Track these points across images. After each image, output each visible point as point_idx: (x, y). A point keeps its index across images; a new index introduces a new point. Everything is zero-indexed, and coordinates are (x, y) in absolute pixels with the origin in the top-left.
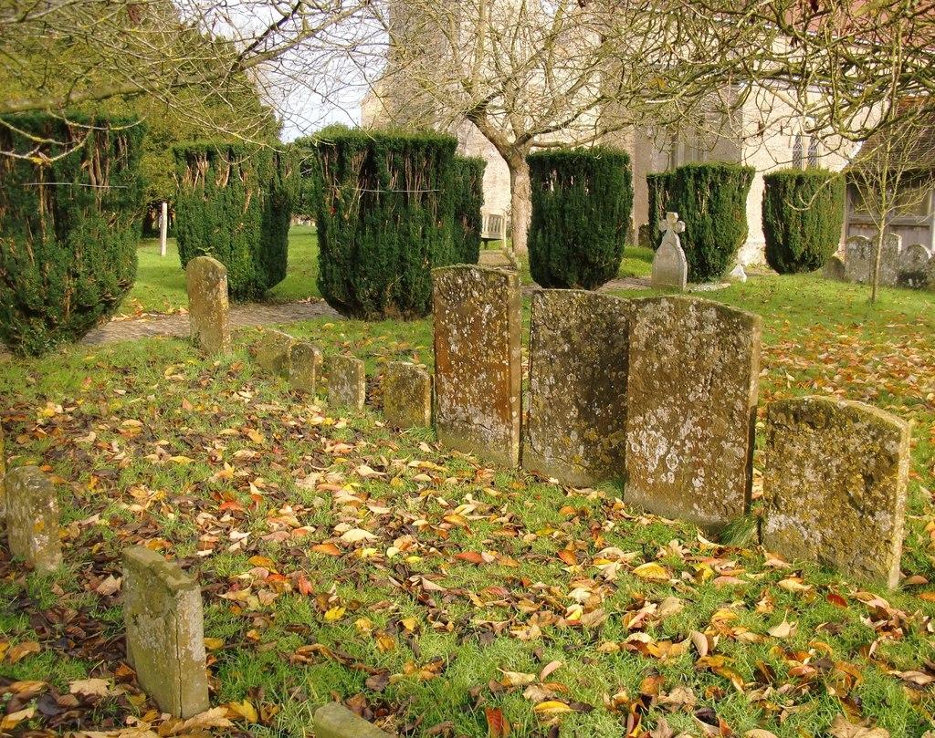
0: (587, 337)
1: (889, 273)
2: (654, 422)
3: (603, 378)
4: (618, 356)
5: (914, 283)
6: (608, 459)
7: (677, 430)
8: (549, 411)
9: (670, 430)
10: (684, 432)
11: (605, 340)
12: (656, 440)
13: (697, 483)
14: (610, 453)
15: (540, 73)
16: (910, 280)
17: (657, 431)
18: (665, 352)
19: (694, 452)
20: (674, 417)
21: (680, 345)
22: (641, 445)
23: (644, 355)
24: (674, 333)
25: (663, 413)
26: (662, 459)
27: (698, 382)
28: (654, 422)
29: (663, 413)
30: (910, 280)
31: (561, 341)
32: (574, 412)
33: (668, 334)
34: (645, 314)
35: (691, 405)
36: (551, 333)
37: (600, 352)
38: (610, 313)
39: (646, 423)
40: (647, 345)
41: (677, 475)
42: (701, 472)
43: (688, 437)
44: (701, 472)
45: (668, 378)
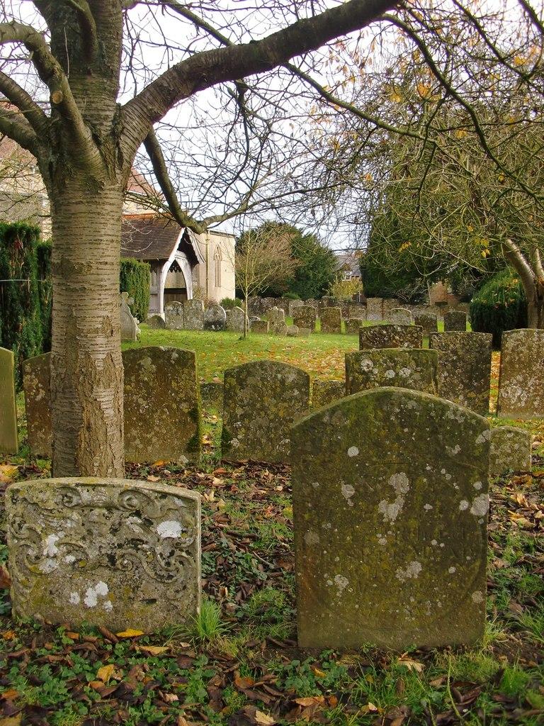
0: (467, 351)
1: (198, 322)
2: (515, 382)
3: (477, 369)
4: (487, 358)
5: (216, 327)
6: (482, 404)
7: (526, 384)
8: (445, 389)
9: (523, 384)
10: (530, 384)
11: (479, 352)
12: (516, 389)
13: (536, 403)
14: (483, 401)
15: (210, 184)
16: (213, 326)
17: (516, 385)
18: (522, 352)
19: (534, 391)
20: (525, 379)
21: (529, 348)
22: (508, 393)
23: (511, 355)
24: (526, 344)
25: (520, 378)
26: (519, 397)
27: (537, 362)
28: (515, 382)
29: (520, 378)
30: (213, 326)
31: (451, 355)
32: (461, 386)
33: (523, 344)
34: (512, 338)
35: (534, 372)
36: (444, 352)
37: (476, 357)
38: (481, 340)
39: (511, 383)
40: (513, 351)
41: (526, 402)
42: (538, 398)
43: (532, 385)
44: (538, 398)
45: (523, 363)
